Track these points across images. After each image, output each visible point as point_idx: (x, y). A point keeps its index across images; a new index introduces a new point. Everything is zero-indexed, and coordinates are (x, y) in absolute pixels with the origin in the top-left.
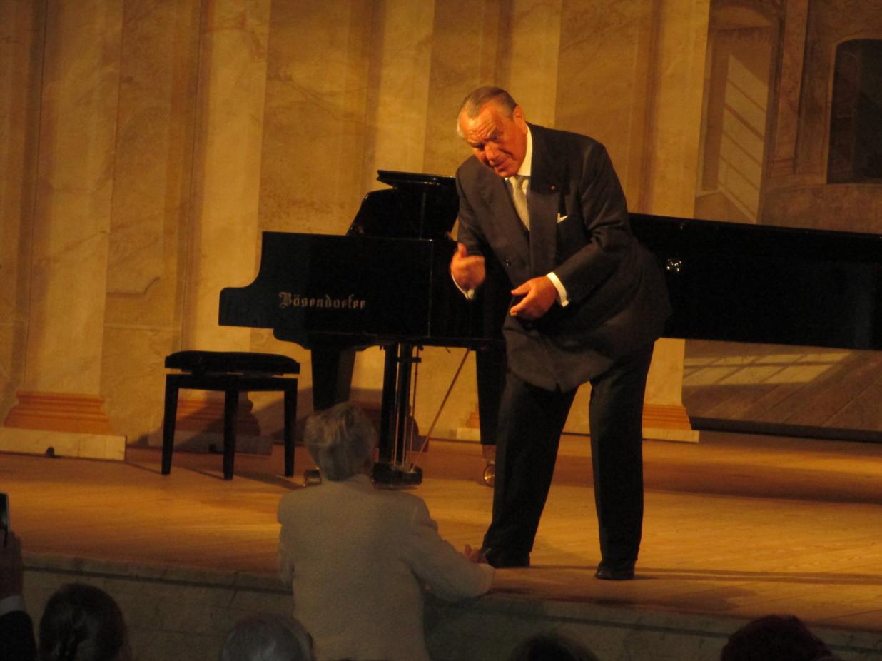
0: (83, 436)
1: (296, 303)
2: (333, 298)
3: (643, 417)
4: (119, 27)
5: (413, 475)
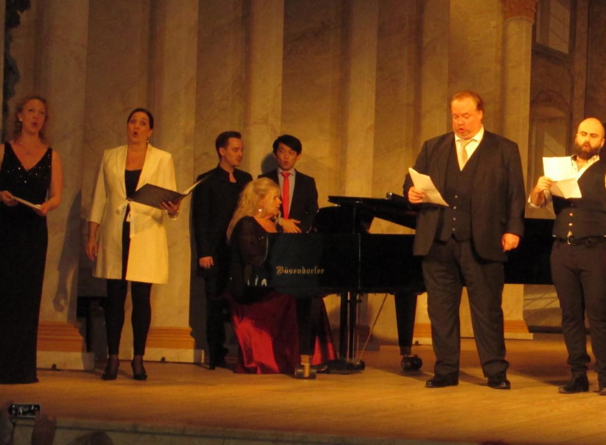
0: (180, 350)
1: (286, 272)
2: (306, 269)
3: (39, 336)
4: (193, 123)
5: (358, 365)
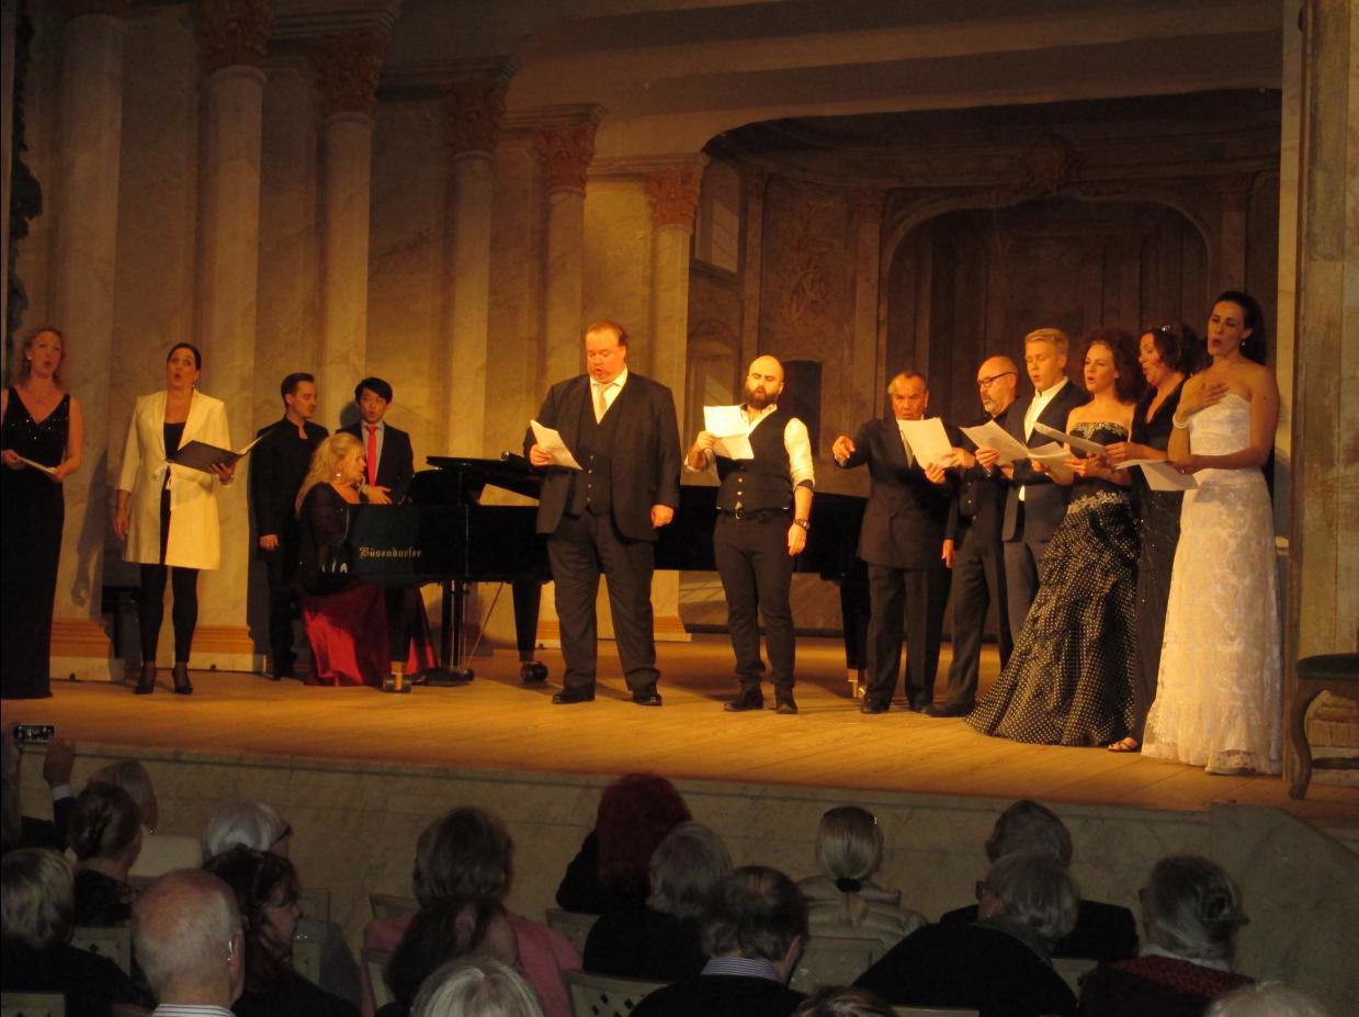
0: (234, 655)
1: (372, 554)
2: (398, 550)
4: (252, 363)
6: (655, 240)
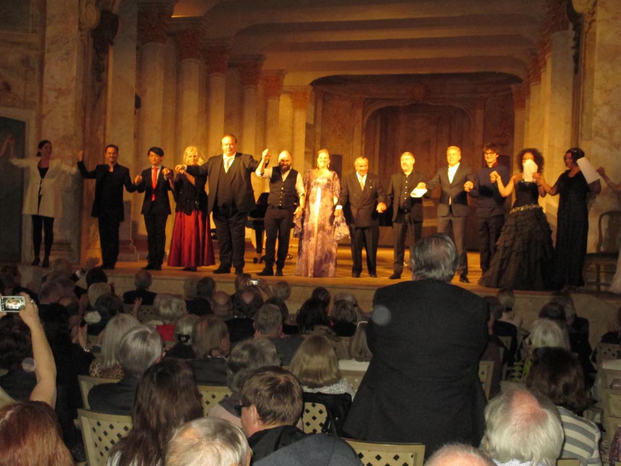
6: (293, 115)
